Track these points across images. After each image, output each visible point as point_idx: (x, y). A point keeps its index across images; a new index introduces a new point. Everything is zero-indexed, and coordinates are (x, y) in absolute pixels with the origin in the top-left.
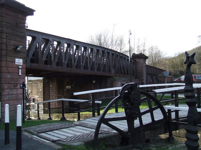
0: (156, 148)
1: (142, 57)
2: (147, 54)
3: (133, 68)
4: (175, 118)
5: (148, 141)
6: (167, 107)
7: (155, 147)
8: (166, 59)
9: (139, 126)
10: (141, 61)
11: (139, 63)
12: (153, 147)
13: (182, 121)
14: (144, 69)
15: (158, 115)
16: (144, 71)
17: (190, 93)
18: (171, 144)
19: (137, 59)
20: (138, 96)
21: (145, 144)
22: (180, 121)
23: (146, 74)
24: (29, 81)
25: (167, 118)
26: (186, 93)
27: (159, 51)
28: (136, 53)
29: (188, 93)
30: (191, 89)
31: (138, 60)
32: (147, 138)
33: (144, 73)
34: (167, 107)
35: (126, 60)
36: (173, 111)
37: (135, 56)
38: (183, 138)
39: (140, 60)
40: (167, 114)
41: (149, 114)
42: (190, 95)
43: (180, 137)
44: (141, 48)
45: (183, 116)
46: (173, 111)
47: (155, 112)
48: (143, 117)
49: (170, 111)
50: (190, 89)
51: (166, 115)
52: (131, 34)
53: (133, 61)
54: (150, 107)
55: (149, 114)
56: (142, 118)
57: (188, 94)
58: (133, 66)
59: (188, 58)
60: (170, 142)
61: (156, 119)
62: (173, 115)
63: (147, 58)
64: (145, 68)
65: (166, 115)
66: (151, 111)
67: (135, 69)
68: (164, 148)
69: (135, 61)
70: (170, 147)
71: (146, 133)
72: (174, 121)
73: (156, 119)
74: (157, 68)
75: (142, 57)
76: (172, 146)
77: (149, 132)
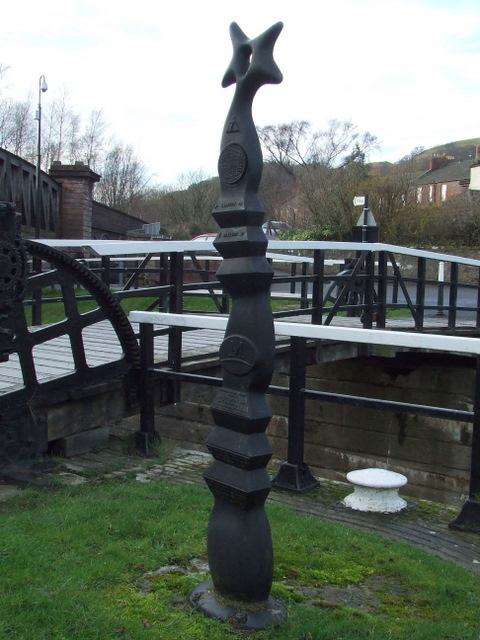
0: (87, 477)
1: (83, 174)
2: (100, 167)
3: (53, 208)
4: (166, 358)
5: (56, 448)
6: (137, 317)
7: (80, 474)
8: (154, 193)
9: (23, 387)
10: (79, 186)
11: (71, 191)
12: (74, 472)
13: (193, 370)
14: (85, 212)
15: (103, 346)
16: (85, 217)
17: (244, 229)
18: (148, 457)
19: (66, 181)
20: (13, 259)
21: (41, 460)
22: (186, 369)
23: (92, 228)
24: (36, 322)
25: (138, 358)
26: (224, 231)
27: (135, 165)
28: (65, 161)
29: (235, 230)
30: (251, 209)
31: (67, 183)
32: (51, 437)
33: (85, 223)
34: (137, 317)
35: (31, 177)
36: (161, 333)
37: (59, 171)
38: (189, 423)
39: (73, 184)
40: (138, 340)
41: (65, 341)
42: (245, 237)
43: (181, 419)
44: (82, 156)
45: (195, 353)
46: (161, 333)
47: (89, 333)
48: (38, 352)
49: (146, 328)
50: (243, 208)
51: (136, 344)
52: (44, 90)
53: (51, 185)
54: (71, 309)
55: (65, 341)
56: (34, 354)
57: (236, 235)
58: (53, 202)
59: (243, 50)
60: (144, 452)
61: (93, 362)
62: (161, 348)
63: (95, 177)
64: (88, 211)
65: (136, 344)
66: (74, 329)
67: (58, 209)
68: (119, 477)
69: (60, 185)
70: (142, 472)
71: (50, 417)
72: (164, 370)
73: (93, 362)
74: (125, 215)
75: (81, 174)
76: (149, 469)
77: (60, 412)
